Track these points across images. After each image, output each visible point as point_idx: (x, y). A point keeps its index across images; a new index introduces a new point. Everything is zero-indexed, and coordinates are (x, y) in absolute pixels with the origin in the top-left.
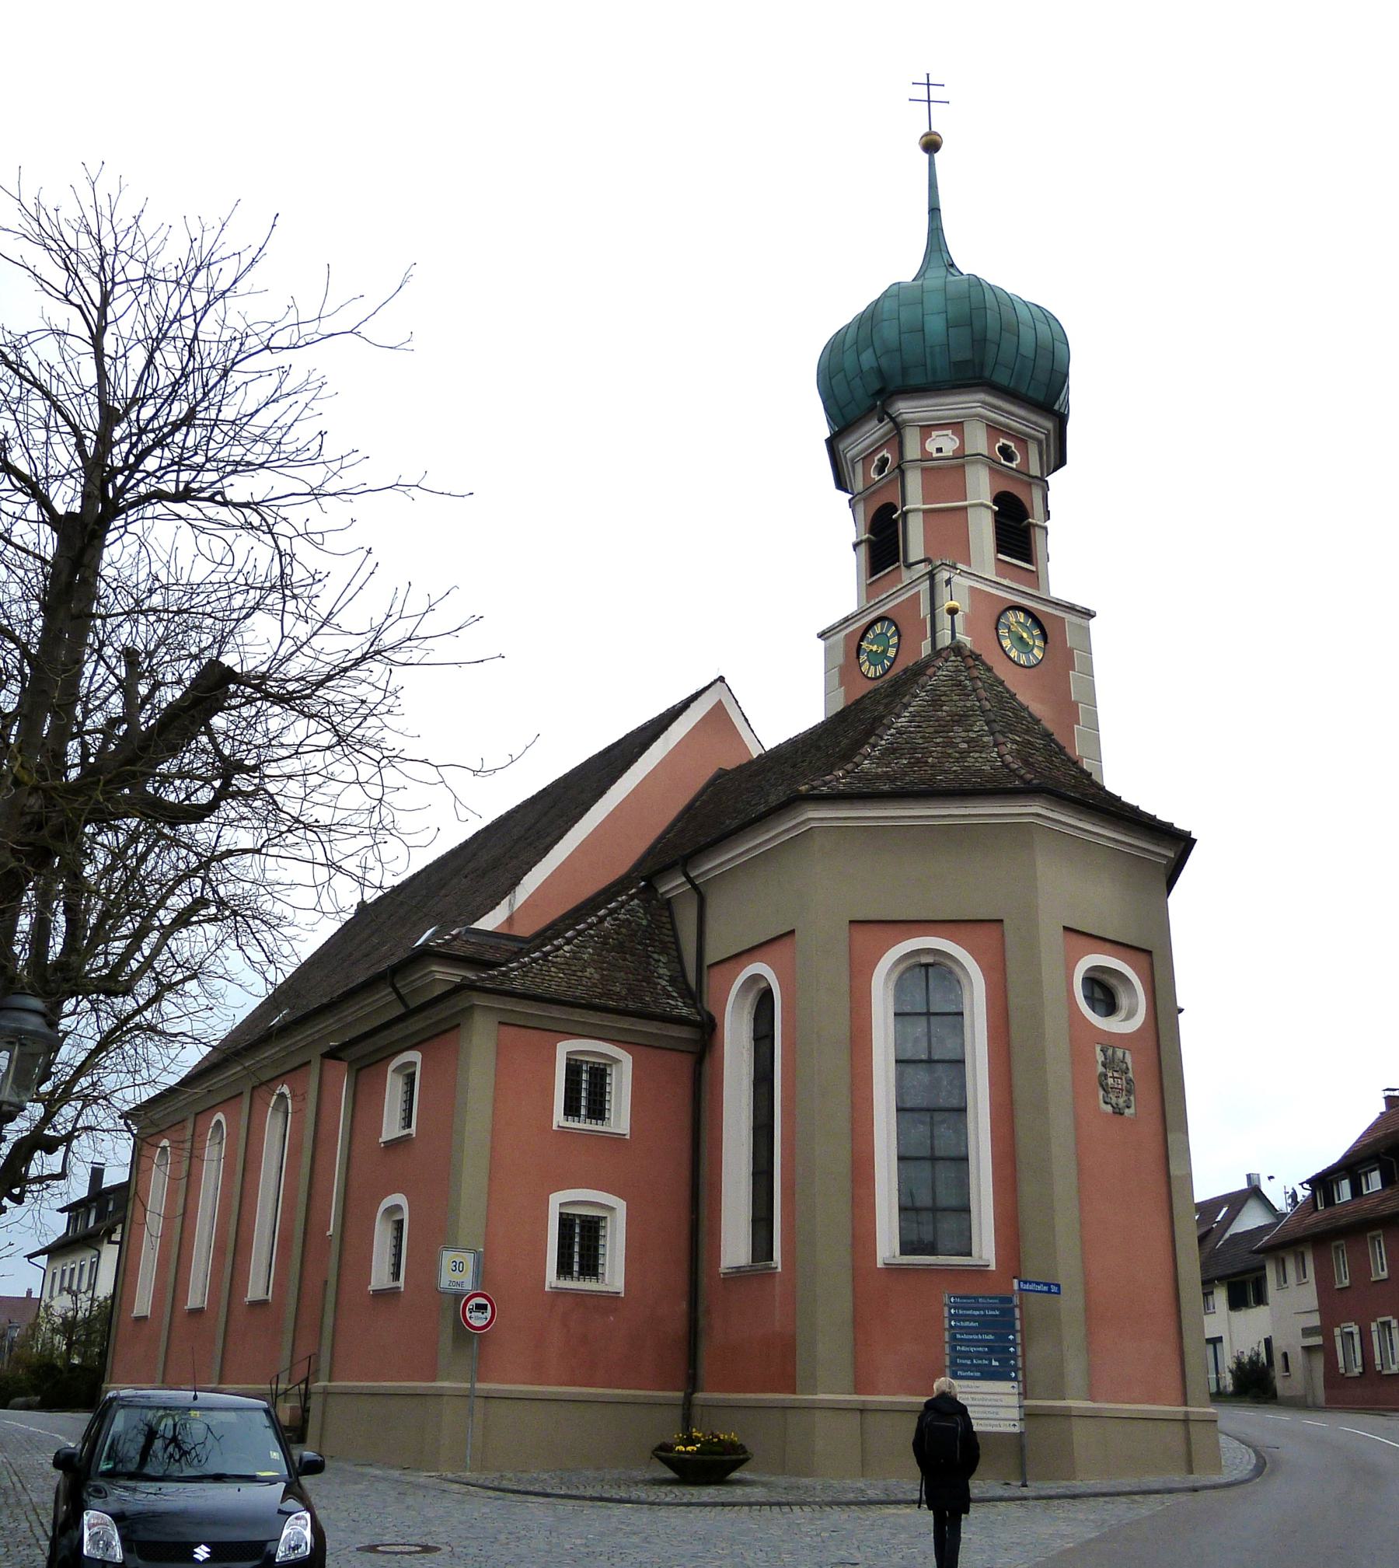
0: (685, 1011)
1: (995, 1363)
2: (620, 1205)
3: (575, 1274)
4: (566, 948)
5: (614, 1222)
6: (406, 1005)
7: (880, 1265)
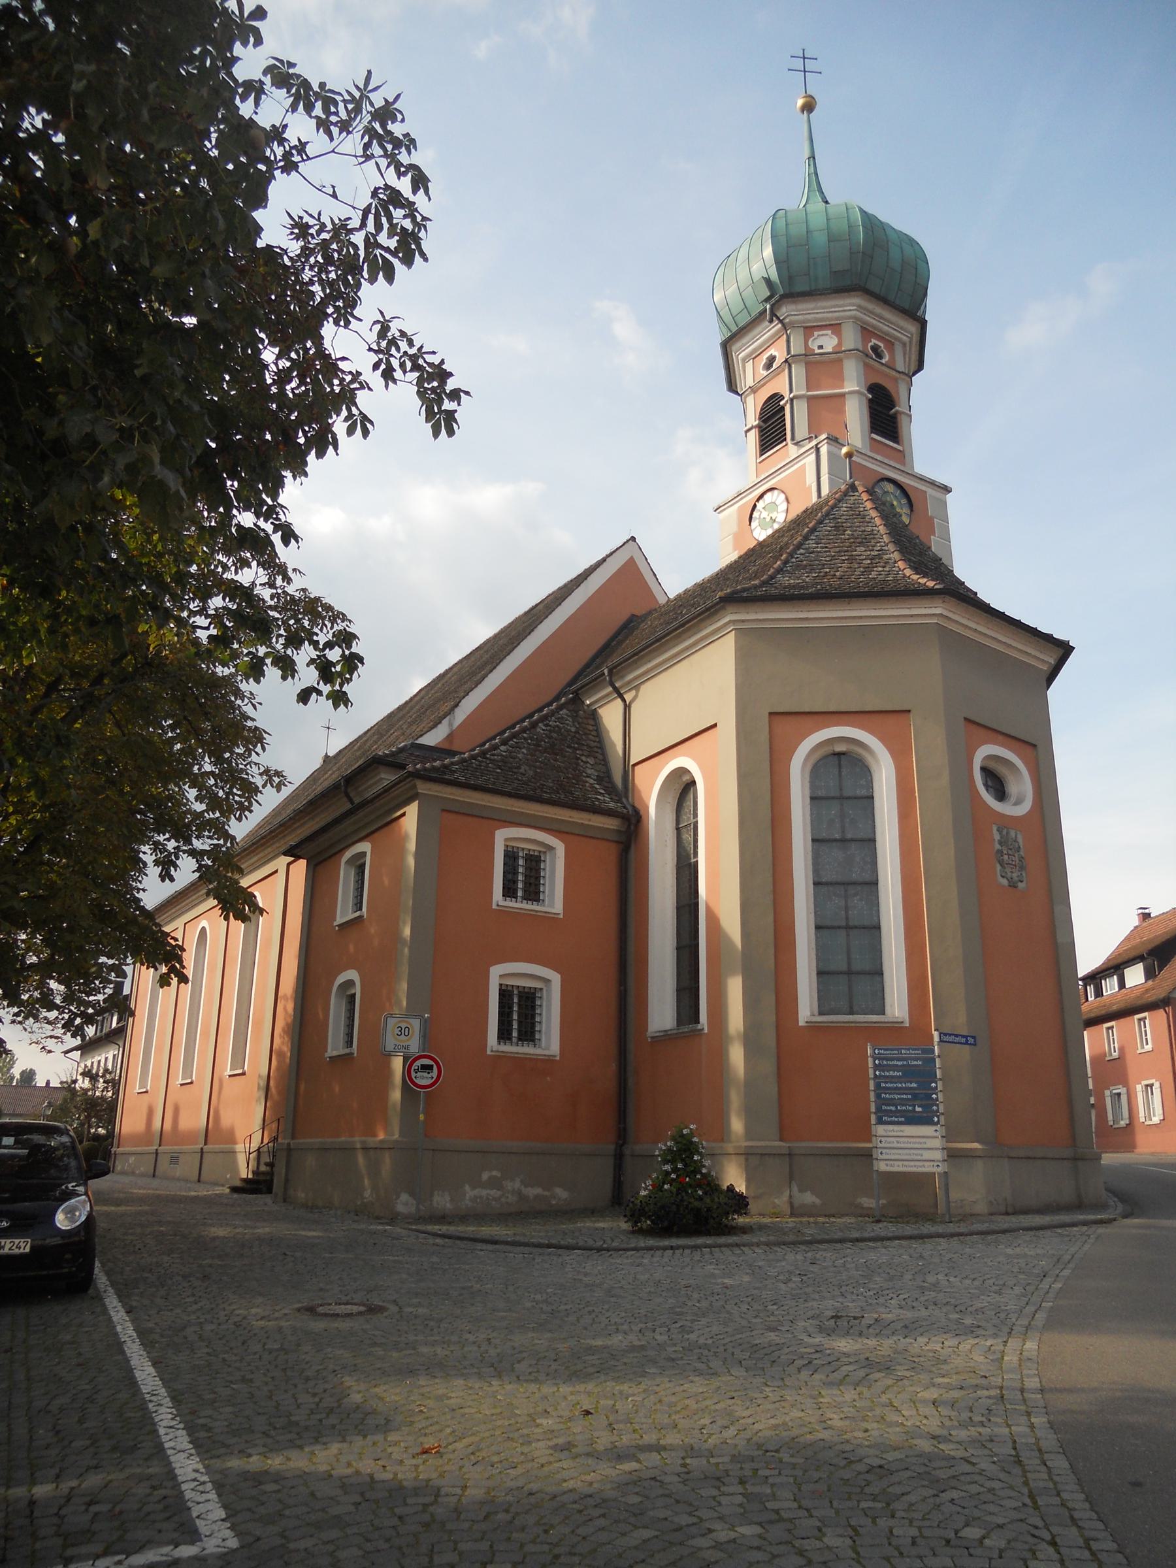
0: (612, 805)
1: (918, 1109)
2: (555, 978)
3: (514, 1040)
4: (503, 748)
5: (549, 991)
6: (352, 802)
7: (801, 1023)
